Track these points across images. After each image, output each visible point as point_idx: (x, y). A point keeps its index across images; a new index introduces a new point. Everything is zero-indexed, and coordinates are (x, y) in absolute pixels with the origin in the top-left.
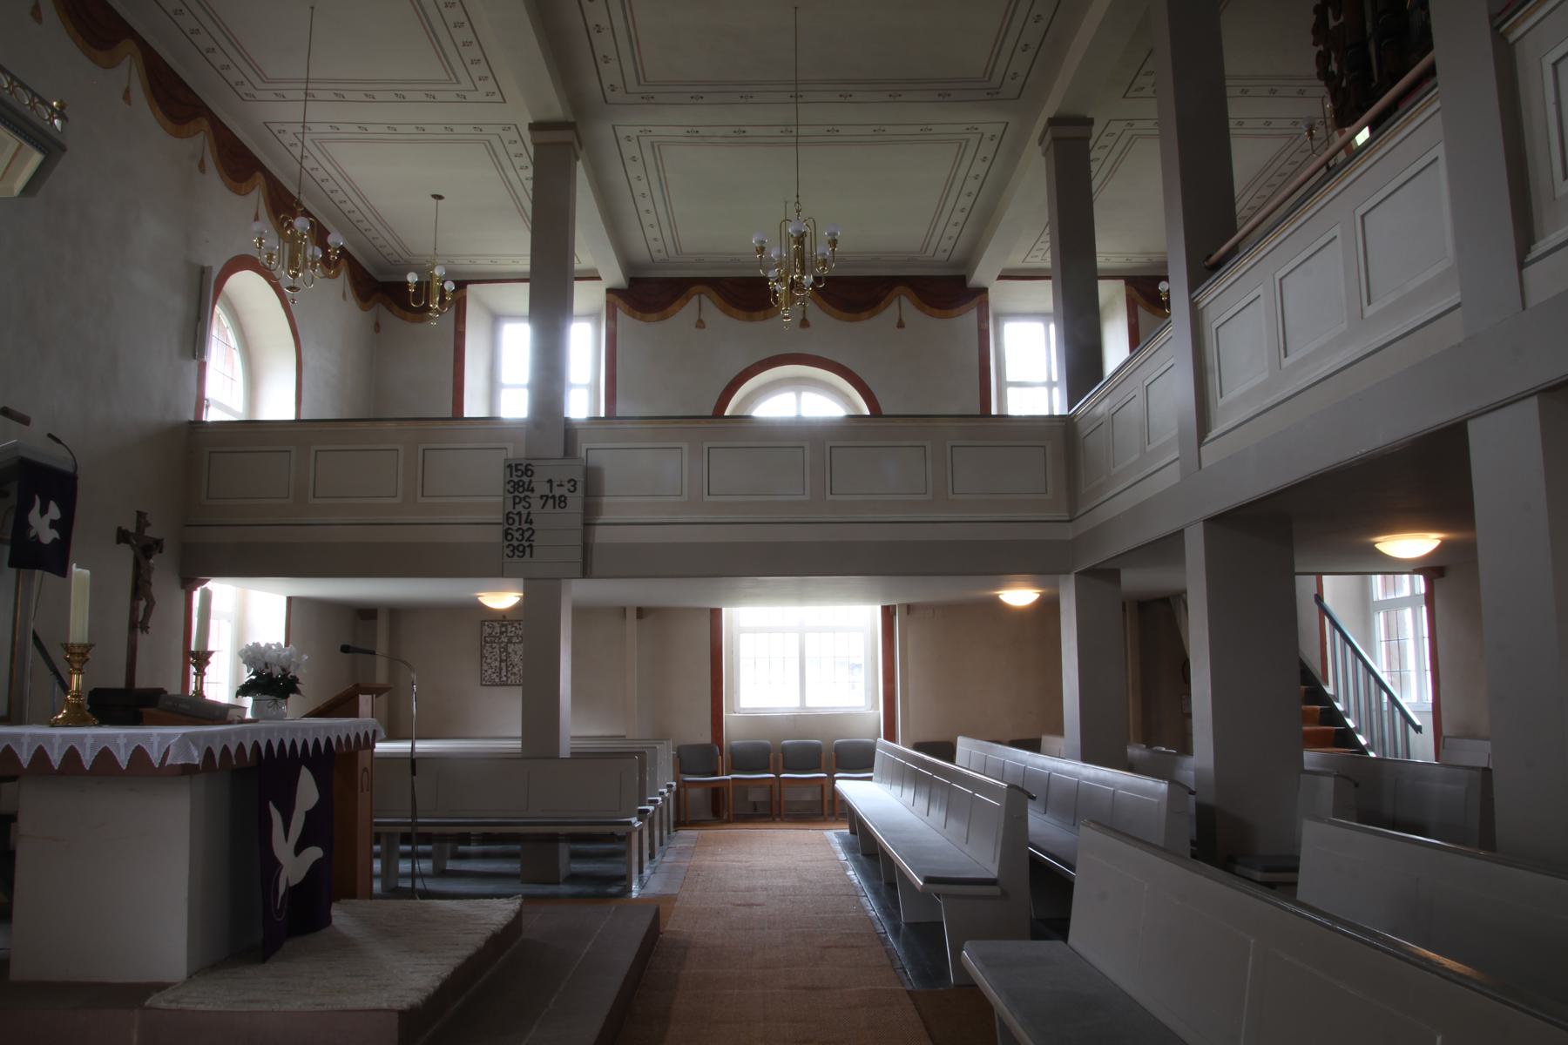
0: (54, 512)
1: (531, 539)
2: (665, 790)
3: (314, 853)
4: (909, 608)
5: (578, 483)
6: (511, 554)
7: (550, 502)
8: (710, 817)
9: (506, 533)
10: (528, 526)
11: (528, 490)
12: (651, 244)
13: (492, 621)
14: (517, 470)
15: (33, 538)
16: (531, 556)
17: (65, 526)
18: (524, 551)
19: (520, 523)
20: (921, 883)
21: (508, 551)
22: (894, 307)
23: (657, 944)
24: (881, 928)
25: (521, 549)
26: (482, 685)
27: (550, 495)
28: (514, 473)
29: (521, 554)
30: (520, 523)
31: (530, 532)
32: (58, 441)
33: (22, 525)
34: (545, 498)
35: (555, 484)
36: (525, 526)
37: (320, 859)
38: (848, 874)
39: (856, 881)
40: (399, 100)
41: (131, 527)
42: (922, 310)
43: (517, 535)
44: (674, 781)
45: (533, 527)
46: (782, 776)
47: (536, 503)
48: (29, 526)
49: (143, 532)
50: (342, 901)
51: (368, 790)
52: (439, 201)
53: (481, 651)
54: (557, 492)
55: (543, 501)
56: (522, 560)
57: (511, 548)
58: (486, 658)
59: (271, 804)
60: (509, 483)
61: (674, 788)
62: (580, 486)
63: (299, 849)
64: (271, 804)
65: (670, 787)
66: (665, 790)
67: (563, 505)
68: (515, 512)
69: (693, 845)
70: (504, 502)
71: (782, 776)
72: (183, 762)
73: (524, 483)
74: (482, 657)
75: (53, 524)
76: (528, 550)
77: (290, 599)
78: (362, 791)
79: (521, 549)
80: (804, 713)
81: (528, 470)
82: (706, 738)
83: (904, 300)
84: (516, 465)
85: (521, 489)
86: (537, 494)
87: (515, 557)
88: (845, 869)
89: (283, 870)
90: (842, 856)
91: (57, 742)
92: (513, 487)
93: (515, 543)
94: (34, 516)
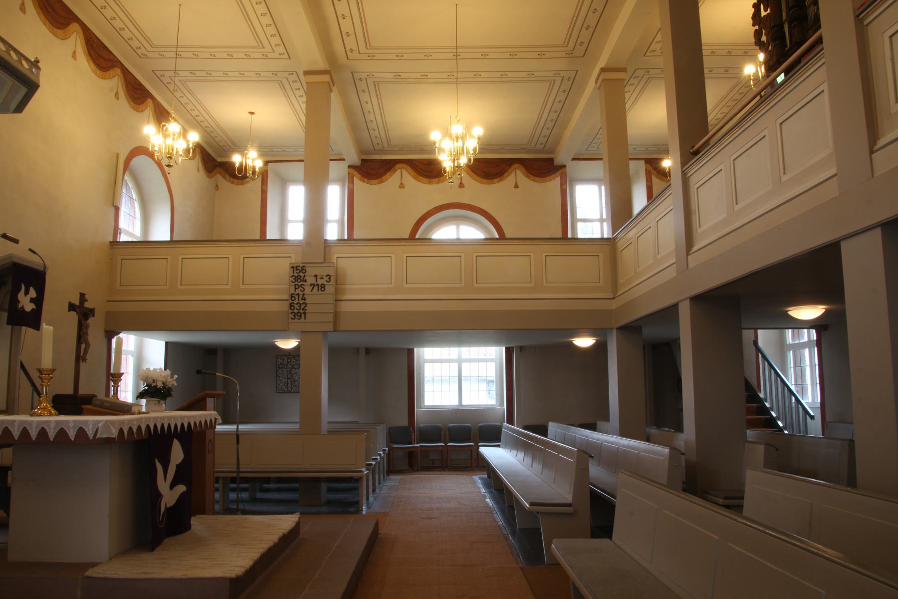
0: (33, 293)
1: (305, 308)
2: (382, 453)
3: (181, 488)
4: (521, 349)
6: (293, 317)
7: (316, 288)
9: (291, 305)
10: (303, 301)
11: (303, 281)
12: (374, 140)
14: (297, 270)
15: (21, 308)
16: (305, 319)
17: (38, 301)
18: (301, 316)
19: (299, 300)
21: (292, 316)
25: (299, 314)
26: (277, 392)
27: (316, 284)
28: (295, 271)
29: (299, 318)
30: (299, 300)
33: (14, 300)
34: (313, 285)
35: (318, 278)
36: (301, 302)
41: (77, 303)
42: (529, 178)
45: (306, 302)
46: (449, 444)
47: (308, 289)
48: (19, 302)
50: (197, 516)
52: (253, 115)
53: (277, 373)
54: (320, 282)
55: (311, 287)
57: (293, 314)
59: (156, 461)
60: (292, 276)
61: (387, 452)
62: (332, 278)
63: (172, 486)
65: (384, 450)
66: (382, 453)
67: (323, 289)
68: (296, 293)
70: (289, 288)
71: (449, 444)
72: (106, 436)
73: (301, 276)
75: (32, 300)
76: (303, 315)
77: (167, 344)
81: (303, 269)
82: (404, 422)
83: (518, 172)
84: (297, 267)
85: (299, 281)
86: (308, 283)
88: (485, 497)
90: (483, 490)
93: (296, 311)
94: (21, 295)
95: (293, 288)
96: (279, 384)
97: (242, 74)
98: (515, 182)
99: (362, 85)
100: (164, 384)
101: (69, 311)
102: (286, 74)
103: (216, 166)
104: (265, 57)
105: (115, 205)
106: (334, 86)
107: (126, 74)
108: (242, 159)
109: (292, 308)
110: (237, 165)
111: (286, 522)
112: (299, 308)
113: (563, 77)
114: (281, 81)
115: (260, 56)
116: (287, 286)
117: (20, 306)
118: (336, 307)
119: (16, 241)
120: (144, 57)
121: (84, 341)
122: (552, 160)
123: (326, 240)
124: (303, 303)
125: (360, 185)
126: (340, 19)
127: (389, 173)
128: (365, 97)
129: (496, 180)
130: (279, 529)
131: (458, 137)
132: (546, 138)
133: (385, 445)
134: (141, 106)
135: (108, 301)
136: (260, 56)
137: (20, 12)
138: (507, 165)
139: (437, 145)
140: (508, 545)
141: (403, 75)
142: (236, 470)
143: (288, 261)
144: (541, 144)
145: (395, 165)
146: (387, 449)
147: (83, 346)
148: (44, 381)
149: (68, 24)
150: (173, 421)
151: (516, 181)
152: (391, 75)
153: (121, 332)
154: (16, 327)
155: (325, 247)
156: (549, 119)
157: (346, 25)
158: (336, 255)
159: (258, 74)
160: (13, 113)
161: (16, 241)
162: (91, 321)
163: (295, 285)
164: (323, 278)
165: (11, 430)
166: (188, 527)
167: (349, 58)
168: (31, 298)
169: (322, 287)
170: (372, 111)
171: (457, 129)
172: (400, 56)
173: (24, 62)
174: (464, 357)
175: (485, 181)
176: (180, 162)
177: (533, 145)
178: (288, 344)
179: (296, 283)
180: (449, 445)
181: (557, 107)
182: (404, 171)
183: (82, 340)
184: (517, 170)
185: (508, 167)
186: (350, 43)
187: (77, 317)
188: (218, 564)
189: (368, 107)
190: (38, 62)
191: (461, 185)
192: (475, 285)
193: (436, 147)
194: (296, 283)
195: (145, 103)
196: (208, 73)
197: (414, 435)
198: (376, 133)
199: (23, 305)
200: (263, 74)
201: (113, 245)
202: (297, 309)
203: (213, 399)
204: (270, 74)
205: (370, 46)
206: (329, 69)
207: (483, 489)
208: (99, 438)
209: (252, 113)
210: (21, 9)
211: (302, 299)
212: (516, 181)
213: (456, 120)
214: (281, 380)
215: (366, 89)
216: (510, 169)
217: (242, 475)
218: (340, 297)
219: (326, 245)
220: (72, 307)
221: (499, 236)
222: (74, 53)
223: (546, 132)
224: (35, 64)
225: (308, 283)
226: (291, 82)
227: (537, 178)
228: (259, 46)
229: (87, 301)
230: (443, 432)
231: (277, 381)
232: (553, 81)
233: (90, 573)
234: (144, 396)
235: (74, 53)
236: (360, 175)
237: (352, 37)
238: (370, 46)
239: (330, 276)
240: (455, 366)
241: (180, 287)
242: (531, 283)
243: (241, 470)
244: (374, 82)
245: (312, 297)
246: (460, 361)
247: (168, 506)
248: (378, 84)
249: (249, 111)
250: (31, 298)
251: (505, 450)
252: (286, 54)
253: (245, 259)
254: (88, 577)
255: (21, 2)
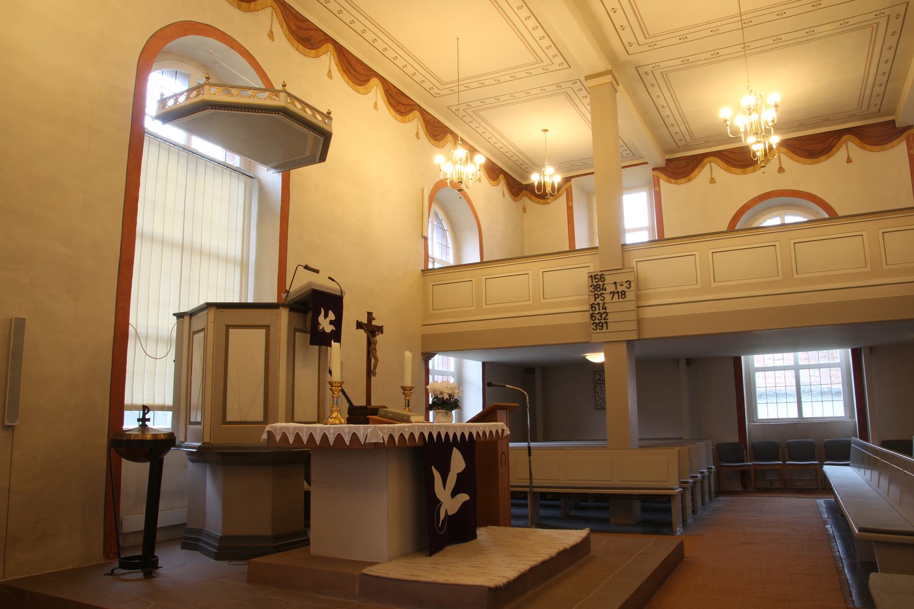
0: (332, 316)
1: (606, 318)
2: (705, 471)
3: (464, 497)
4: (871, 349)
5: (632, 282)
6: (595, 328)
7: (616, 295)
8: (740, 488)
9: (592, 316)
10: (604, 311)
11: (603, 290)
12: (675, 136)
13: (600, 371)
14: (595, 279)
15: (321, 330)
16: (607, 329)
17: (337, 323)
18: (602, 326)
19: (599, 310)
20: (857, 532)
21: (593, 326)
22: (843, 149)
23: (679, 566)
24: (841, 564)
25: (601, 324)
26: (596, 409)
27: (616, 291)
28: (594, 280)
29: (601, 328)
30: (599, 310)
31: (605, 314)
32: (333, 280)
33: (316, 323)
34: (613, 293)
35: (618, 285)
36: (602, 311)
37: (467, 501)
38: (826, 527)
39: (831, 532)
40: (497, 83)
41: (365, 321)
42: (864, 149)
43: (598, 316)
44: (714, 465)
45: (607, 311)
46: (787, 462)
47: (608, 298)
48: (319, 324)
49: (372, 323)
50: (489, 527)
51: (506, 464)
52: (546, 133)
53: (595, 389)
54: (620, 289)
55: (612, 295)
56: (602, 331)
57: (595, 325)
58: (597, 393)
59: (433, 467)
60: (591, 286)
61: (713, 470)
62: (633, 284)
63: (453, 494)
64: (433, 467)
65: (709, 469)
66: (705, 471)
67: (623, 296)
68: (596, 303)
69: (725, 505)
70: (589, 298)
71: (787, 462)
72: (375, 441)
73: (600, 285)
74: (595, 393)
75: (331, 322)
76: (605, 325)
77: (484, 364)
78: (501, 465)
79: (601, 324)
80: (801, 421)
81: (602, 277)
82: (736, 439)
83: (850, 144)
84: (595, 275)
85: (598, 290)
86: (608, 291)
87: (598, 330)
88: (825, 523)
89: (442, 505)
90: (825, 516)
91: (305, 430)
92: (594, 288)
93: (597, 321)
94: (321, 318)
95: (593, 297)
96: (598, 401)
97: (527, 93)
98: (847, 156)
99: (649, 79)
100: (450, 395)
101: (357, 329)
102: (570, 84)
103: (522, 190)
104: (547, 71)
105: (423, 235)
106: (618, 85)
107: (423, 113)
108: (541, 177)
109: (594, 318)
110: (536, 184)
111: (572, 537)
112: (600, 318)
113: (889, 16)
114: (566, 92)
115: (541, 71)
116: (587, 296)
117: (321, 328)
118: (638, 314)
119: (317, 272)
120: (437, 96)
121: (373, 356)
122: (893, 122)
123: (624, 245)
124: (604, 313)
125: (667, 187)
126: (611, 13)
127: (697, 169)
128: (655, 91)
129: (822, 158)
130: (562, 543)
131: (750, 109)
132: (881, 97)
133: (712, 464)
134: (441, 142)
135: (423, 325)
136: (541, 71)
137: (327, 78)
138: (836, 138)
139: (728, 123)
140: (839, 580)
141: (691, 59)
142: (529, 484)
143: (587, 270)
144: (876, 105)
145: (703, 160)
146: (713, 467)
147: (373, 361)
148: (335, 392)
149: (368, 81)
150: (451, 429)
151: (848, 155)
152: (678, 62)
153: (436, 354)
154: (323, 347)
155: (623, 252)
156: (880, 72)
157: (619, 19)
158: (633, 259)
159: (543, 89)
160: (319, 163)
161: (317, 272)
162: (379, 338)
163: (595, 294)
164: (623, 285)
165: (301, 436)
166: (474, 536)
167: (630, 53)
168: (330, 320)
169: (623, 294)
170: (665, 104)
171: (747, 100)
172: (684, 39)
173: (318, 116)
174: (801, 363)
175: (809, 160)
176: (471, 185)
177: (865, 108)
178: (597, 358)
179: (596, 292)
180: (787, 464)
181: (888, 55)
182: (714, 165)
183: (371, 355)
184: (848, 142)
185: (836, 140)
186: (627, 36)
187: (366, 335)
188: (483, 573)
189: (661, 102)
190: (329, 113)
191: (781, 170)
192: (796, 276)
193: (727, 125)
194: (596, 292)
195: (445, 139)
196: (497, 98)
197: (747, 451)
198: (676, 129)
199: (323, 327)
200: (547, 89)
201: (423, 273)
202: (598, 319)
203: (505, 411)
204: (554, 87)
205: (649, 35)
206: (610, 68)
207: (826, 515)
208: (369, 443)
209: (546, 131)
210: (328, 76)
211: (603, 309)
212: (848, 155)
213: (748, 91)
214: (599, 396)
215: (655, 82)
216: (838, 143)
217: (535, 490)
218: (642, 303)
219: (623, 250)
220: (359, 325)
221: (829, 215)
222: (376, 104)
223: (879, 90)
224: (328, 116)
225: (608, 291)
226: (576, 91)
227: (875, 148)
228: (538, 61)
229: (375, 319)
230: (780, 449)
231: (595, 398)
232: (875, 25)
233: (367, 571)
234: (432, 407)
235: (376, 104)
236: (666, 177)
237: (628, 29)
238: (649, 35)
239: (630, 282)
240: (791, 374)
241: (485, 307)
242: (866, 267)
243: (534, 485)
244: (662, 73)
245: (613, 306)
246: (797, 368)
247: (450, 513)
248: (666, 74)
249: (543, 129)
250: (330, 320)
251: (854, 468)
252: (565, 63)
253: (544, 273)
254: (364, 574)
255: (328, 70)
